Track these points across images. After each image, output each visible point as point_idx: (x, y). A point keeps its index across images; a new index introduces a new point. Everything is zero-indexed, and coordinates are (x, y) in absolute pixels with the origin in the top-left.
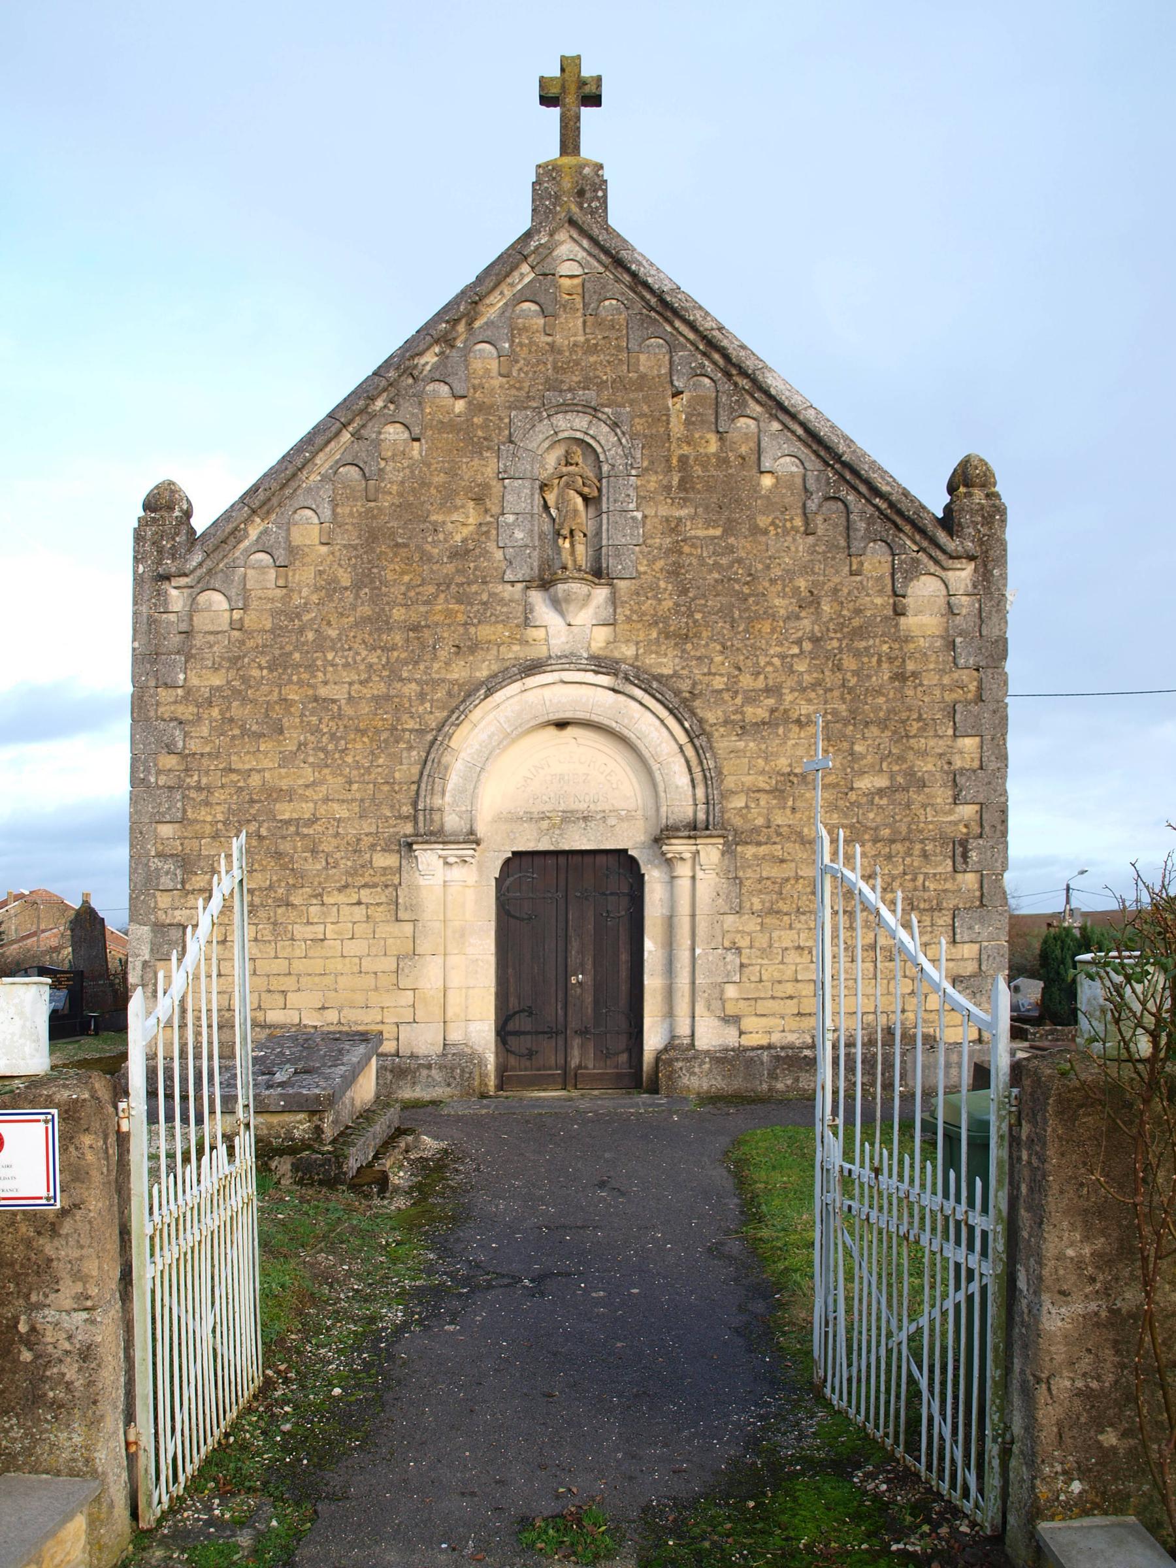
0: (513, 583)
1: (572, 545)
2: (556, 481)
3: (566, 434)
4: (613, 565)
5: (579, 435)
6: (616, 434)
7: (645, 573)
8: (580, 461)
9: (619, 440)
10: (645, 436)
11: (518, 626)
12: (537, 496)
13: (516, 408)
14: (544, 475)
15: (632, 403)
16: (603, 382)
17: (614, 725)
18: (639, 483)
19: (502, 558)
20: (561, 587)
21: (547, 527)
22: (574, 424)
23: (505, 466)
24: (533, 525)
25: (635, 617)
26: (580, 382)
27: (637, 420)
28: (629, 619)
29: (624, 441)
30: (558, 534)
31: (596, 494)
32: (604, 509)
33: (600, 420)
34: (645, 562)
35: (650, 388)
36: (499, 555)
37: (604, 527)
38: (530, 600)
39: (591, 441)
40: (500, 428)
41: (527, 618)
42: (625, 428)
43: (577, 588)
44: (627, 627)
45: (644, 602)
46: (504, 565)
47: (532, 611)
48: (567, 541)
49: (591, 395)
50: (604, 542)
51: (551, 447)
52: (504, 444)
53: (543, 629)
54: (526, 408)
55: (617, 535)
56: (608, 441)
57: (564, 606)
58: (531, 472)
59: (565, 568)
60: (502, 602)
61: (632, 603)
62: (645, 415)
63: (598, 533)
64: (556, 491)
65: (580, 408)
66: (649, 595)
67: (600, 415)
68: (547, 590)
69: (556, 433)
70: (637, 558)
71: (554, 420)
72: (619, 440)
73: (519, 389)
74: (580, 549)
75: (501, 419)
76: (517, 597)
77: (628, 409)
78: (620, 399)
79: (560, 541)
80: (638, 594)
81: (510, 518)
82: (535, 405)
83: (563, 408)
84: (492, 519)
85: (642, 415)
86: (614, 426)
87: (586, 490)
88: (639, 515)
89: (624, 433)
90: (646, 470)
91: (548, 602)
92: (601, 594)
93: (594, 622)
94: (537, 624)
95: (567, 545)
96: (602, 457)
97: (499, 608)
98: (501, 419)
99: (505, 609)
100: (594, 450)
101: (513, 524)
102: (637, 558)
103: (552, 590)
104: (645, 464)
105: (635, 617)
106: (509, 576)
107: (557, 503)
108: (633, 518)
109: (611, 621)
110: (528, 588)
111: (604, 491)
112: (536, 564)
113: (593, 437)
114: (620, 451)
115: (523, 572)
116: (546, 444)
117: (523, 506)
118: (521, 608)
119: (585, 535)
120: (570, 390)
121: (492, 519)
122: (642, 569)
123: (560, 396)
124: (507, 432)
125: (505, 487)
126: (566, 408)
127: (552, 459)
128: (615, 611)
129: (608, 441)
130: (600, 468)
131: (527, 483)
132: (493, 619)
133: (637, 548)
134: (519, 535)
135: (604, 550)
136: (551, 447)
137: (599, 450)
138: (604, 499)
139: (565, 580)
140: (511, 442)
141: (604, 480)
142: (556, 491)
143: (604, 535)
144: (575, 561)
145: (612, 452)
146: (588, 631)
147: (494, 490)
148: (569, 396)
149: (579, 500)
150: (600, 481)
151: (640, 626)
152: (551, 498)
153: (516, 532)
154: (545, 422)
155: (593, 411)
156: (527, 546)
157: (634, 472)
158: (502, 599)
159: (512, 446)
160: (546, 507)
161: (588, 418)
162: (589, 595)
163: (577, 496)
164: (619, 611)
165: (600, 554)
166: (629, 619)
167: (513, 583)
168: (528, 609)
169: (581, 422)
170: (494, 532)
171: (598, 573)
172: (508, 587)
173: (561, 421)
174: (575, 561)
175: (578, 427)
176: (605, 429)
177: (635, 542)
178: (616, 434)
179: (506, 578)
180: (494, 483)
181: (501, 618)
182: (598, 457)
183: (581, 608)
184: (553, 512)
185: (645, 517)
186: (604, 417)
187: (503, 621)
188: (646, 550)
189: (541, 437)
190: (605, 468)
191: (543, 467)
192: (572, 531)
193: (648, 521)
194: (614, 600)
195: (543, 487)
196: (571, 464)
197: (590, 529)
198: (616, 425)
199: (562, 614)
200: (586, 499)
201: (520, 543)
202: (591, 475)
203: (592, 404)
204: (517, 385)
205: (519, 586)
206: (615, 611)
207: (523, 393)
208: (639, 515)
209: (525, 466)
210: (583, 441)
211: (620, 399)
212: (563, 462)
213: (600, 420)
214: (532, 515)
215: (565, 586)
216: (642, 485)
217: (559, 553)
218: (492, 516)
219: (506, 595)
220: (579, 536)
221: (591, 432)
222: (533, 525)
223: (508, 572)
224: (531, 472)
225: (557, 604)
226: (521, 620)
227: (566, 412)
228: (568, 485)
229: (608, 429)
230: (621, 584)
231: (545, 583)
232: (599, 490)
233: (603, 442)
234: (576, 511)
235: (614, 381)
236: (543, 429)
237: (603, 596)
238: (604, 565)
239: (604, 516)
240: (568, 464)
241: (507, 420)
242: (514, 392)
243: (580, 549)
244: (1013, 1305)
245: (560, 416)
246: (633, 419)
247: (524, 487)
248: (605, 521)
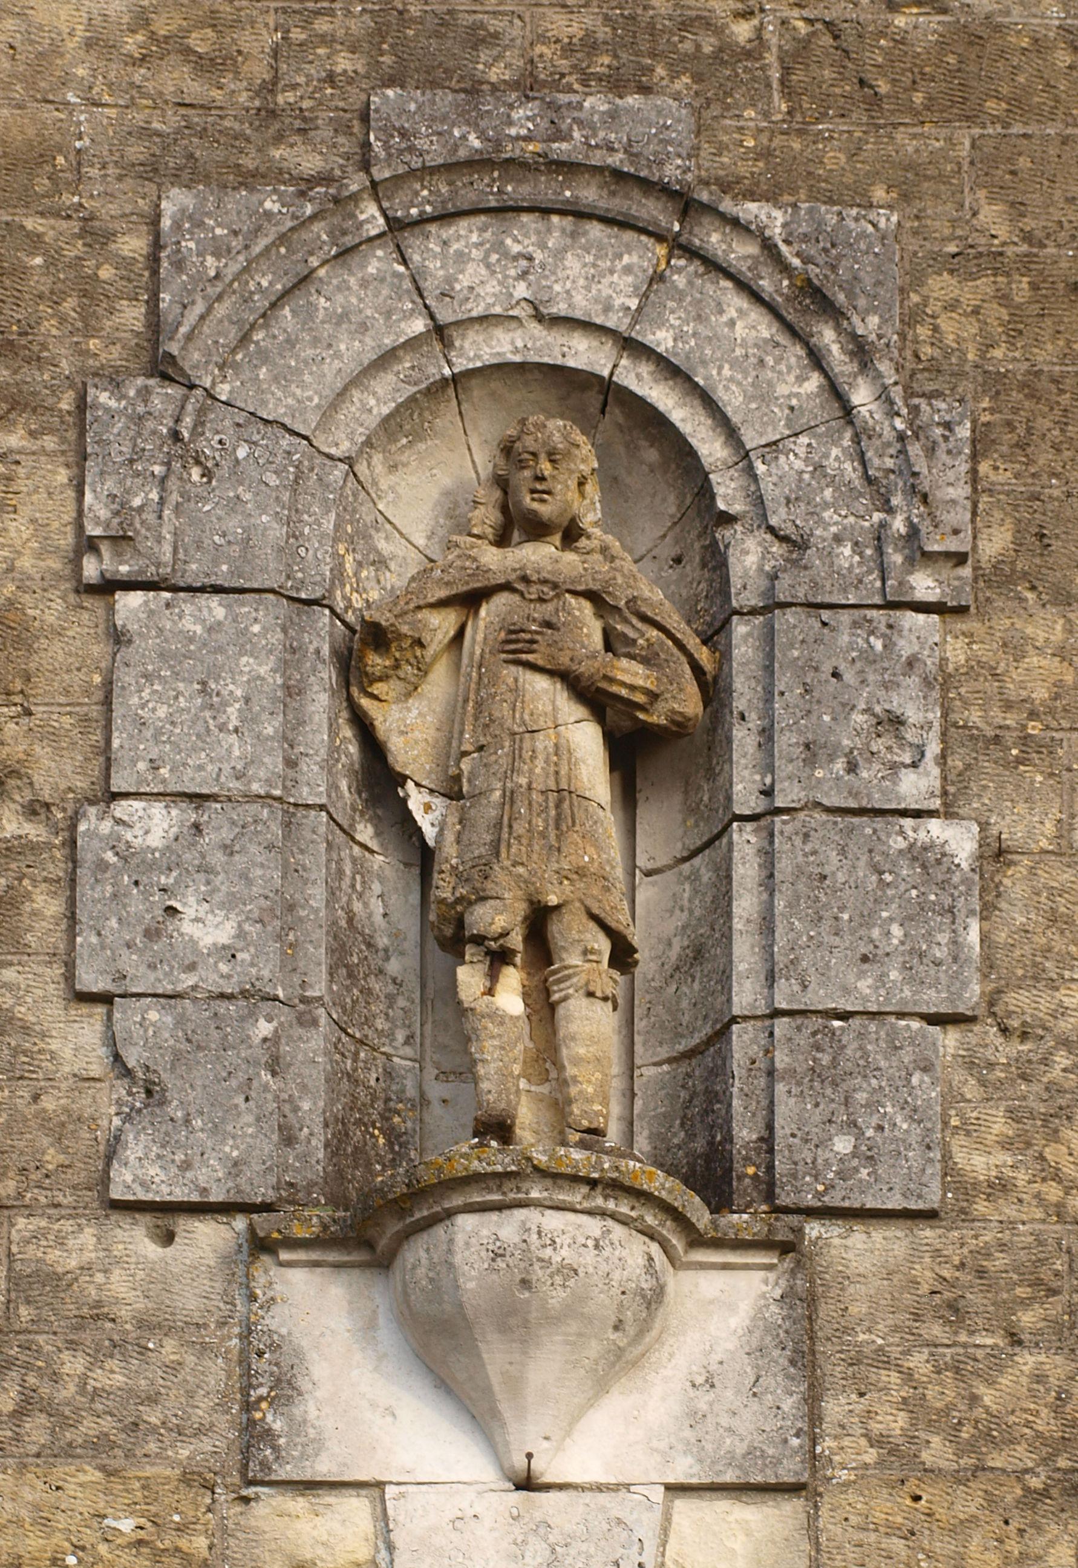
0: (165, 1215)
1: (544, 1007)
2: (441, 625)
3: (502, 346)
4: (815, 1143)
5: (584, 354)
6: (816, 359)
7: (1000, 1187)
8: (590, 517)
9: (835, 392)
10: (994, 383)
11: (198, 1480)
12: (321, 701)
13: (191, 174)
14: (368, 595)
15: (910, 183)
16: (728, 54)
17: (654, 1333)
18: (957, 653)
19: (97, 1062)
20: (474, 1238)
21: (384, 900)
22: (559, 286)
23: (121, 507)
24: (292, 872)
25: (936, 1451)
26: (590, 45)
27: (941, 286)
28: (898, 1460)
29: (861, 396)
30: (453, 938)
31: (688, 702)
32: (745, 794)
33: (714, 267)
34: (999, 1126)
35: (1018, 105)
36: (76, 1042)
37: (745, 905)
38: (275, 1321)
39: (662, 397)
40: (89, 291)
41: (253, 1435)
42: (869, 326)
43: (587, 1247)
44: (889, 1506)
45: (998, 1362)
46: (107, 1104)
47: (285, 1389)
48: (512, 979)
49: (655, 122)
50: (745, 996)
51: (401, 426)
52: (114, 381)
53: (356, 1509)
54: (249, 180)
55: (817, 943)
56: (763, 395)
57: (495, 1356)
58: (291, 546)
59: (498, 1128)
60: (91, 1324)
61: (919, 1361)
62: (993, 261)
63: (704, 953)
64: (439, 683)
65: (590, 194)
66: (1027, 1319)
67: (714, 240)
68: (382, 1262)
69: (440, 332)
70: (952, 1098)
71: (430, 252)
72: (835, 392)
73: (208, 66)
74: (591, 1026)
75: (95, 235)
76: (189, 1301)
77: (887, 220)
78: (834, 158)
79: (470, 978)
80: (955, 1312)
81: (154, 825)
82: (311, 163)
83: (485, 188)
84: (34, 831)
85: (967, 261)
86: (805, 305)
87: (631, 674)
88: (959, 841)
89: (862, 352)
90: (1000, 578)
91: (387, 1335)
92: (725, 1303)
93: (683, 1470)
94: (323, 1468)
95: (511, 997)
96: (728, 493)
97: (73, 1364)
98: (95, 235)
99: (112, 1376)
100: (681, 452)
101: (169, 859)
102: (952, 1098)
103: (418, 1254)
104: (995, 543)
105: (936, 1451)
106: (141, 1171)
107: (449, 751)
108: (928, 859)
109: (790, 1470)
110: (261, 1246)
111: (744, 692)
112: (311, 1109)
113: (670, 370)
114: (838, 457)
115: (228, 1153)
116: (382, 397)
117: (230, 756)
118: (216, 1373)
119: (623, 955)
120: (528, 85)
121: (34, 831)
122: (979, 1163)
123: (471, 117)
124: (132, 316)
125: (118, 637)
126: (507, 186)
127: (418, 504)
128: (813, 1401)
129: (763, 395)
130: (716, 561)
131: (261, 620)
132: (36, 1430)
133: (950, 1040)
134: (205, 927)
135: (743, 1042)
136: (401, 426)
137: (711, 449)
138: (744, 739)
139: (500, 1190)
140: (164, 369)
141: (740, 629)
142: (439, 683)
143: (745, 954)
144: (559, 1106)
145: (792, 463)
146: (647, 1525)
147: (52, 654)
148: (524, 118)
149: (586, 741)
150: (715, 635)
151: (968, 1503)
152: (411, 726)
153: (190, 906)
154: (378, 262)
155: (674, 214)
156: (254, 996)
157: (924, 585)
158: (98, 1314)
159: (163, 397)
160: (379, 778)
161: (642, 255)
162: (653, 1299)
163: (570, 710)
164: (834, 1408)
165: (720, 1071)
166: (898, 1460)
167: (165, 1215)
168: (262, 1381)
169: (598, 276)
170: (47, 905)
171: (713, 1179)
172: (136, 1239)
173: (470, 265)
174: (559, 1106)
175: (581, 305)
176: (751, 326)
177: (934, 1001)
178: (816, 359)
179: (124, 1182)
180: (50, 609)
181: (89, 1427)
182: (705, 492)
183: (601, 1384)
184: (426, 811)
185: (996, 854)
186: (740, 252)
187: (100, 1445)
188: (1005, 1051)
189: (354, 350)
190: (749, 557)
191: (357, 534)
192: (539, 920)
193: (1015, 882)
194: (804, 1341)
195: (368, 650)
196: (537, 529)
197: (655, 918)
198: (817, 299)
199: (476, 1407)
200: (634, 748)
201: (215, 976)
202: (653, 595)
203: (671, 172)
204: (200, 42)
205: (207, 1240)
206: (813, 1401)
207: (237, 93)
208: (959, 841)
209: (241, 517)
210: (609, 392)
211: (834, 158)
212: (487, 517)
213: (714, 267)
214: (292, 811)
215: (507, 1227)
216: (973, 669)
217: (465, 1071)
218: (34, 810)
219: (122, 1290)
220: (581, 949)
221: (662, 339)
222: (292, 872)
223: (134, 1149)
224: (291, 546)
225: (446, 1351)
226: (217, 1444)
227: (505, 210)
228: (516, 647)
229: (765, 328)
230: (855, 1252)
231: (372, 1214)
232: (713, 689)
233: (732, 400)
234: (564, 797)
235: (797, 54)
236: (364, 306)
237: (739, 1319)
238: (745, 1133)
239: (745, 841)
240: (516, 524)
241: (133, 245)
242: (175, 79)
243: (591, 1026)
244: (703, 401)
245: (467, 234)
246: (917, 279)
247: (244, 643)
248: (746, 870)
